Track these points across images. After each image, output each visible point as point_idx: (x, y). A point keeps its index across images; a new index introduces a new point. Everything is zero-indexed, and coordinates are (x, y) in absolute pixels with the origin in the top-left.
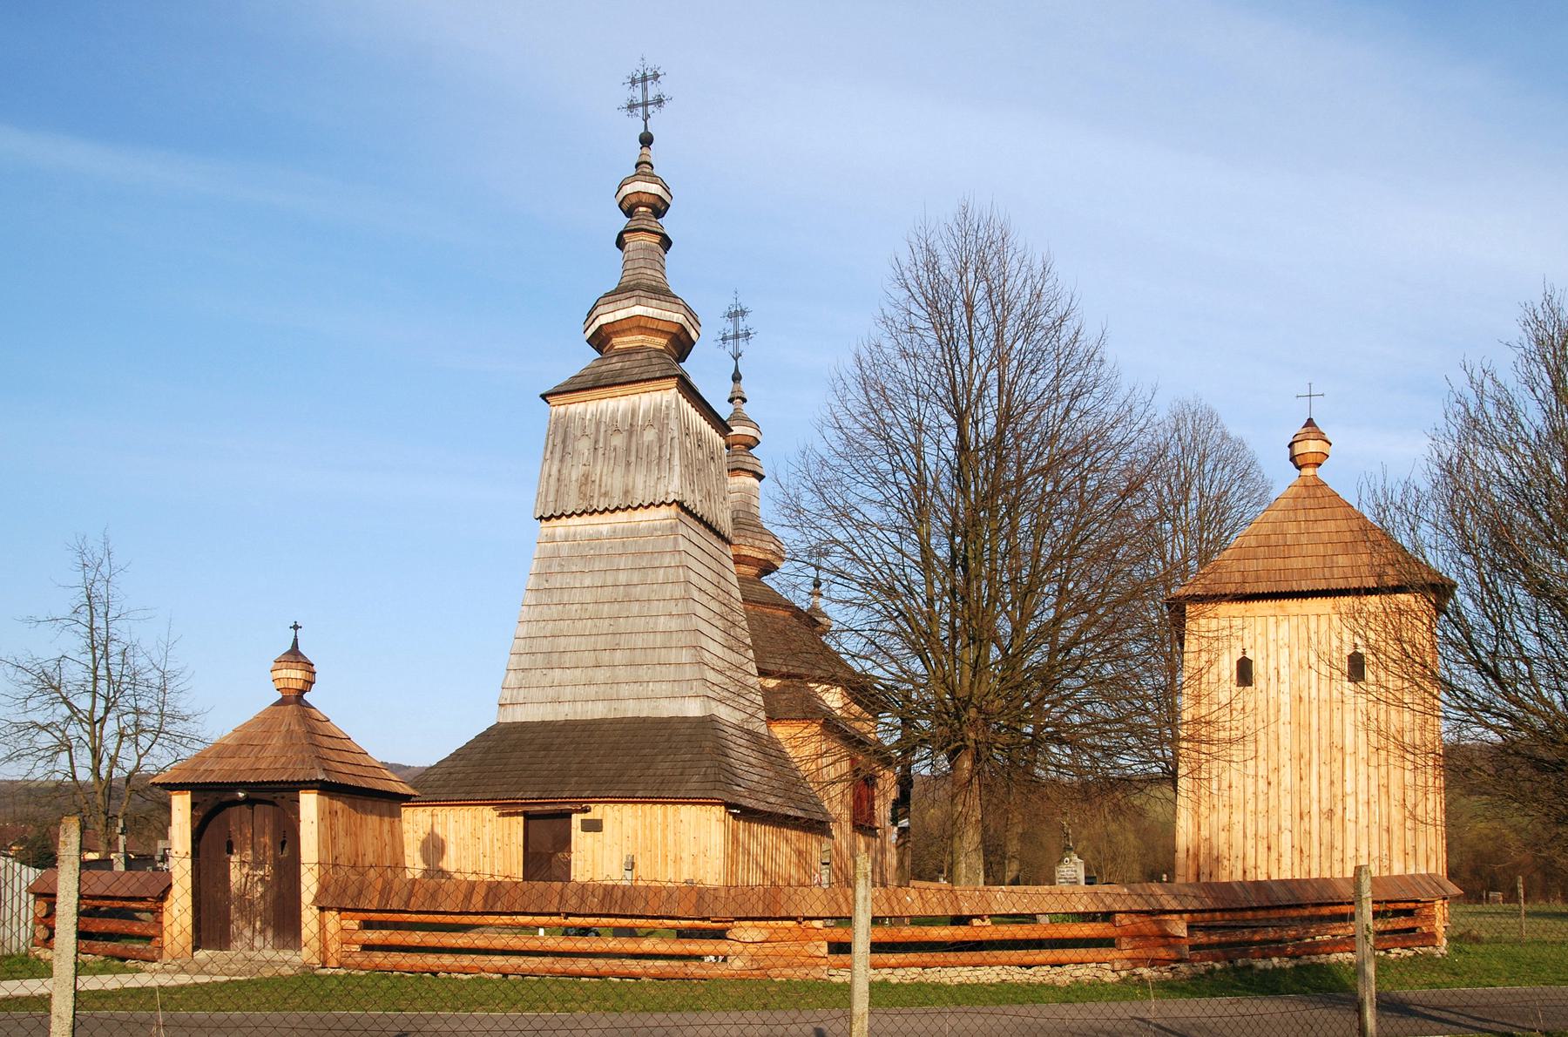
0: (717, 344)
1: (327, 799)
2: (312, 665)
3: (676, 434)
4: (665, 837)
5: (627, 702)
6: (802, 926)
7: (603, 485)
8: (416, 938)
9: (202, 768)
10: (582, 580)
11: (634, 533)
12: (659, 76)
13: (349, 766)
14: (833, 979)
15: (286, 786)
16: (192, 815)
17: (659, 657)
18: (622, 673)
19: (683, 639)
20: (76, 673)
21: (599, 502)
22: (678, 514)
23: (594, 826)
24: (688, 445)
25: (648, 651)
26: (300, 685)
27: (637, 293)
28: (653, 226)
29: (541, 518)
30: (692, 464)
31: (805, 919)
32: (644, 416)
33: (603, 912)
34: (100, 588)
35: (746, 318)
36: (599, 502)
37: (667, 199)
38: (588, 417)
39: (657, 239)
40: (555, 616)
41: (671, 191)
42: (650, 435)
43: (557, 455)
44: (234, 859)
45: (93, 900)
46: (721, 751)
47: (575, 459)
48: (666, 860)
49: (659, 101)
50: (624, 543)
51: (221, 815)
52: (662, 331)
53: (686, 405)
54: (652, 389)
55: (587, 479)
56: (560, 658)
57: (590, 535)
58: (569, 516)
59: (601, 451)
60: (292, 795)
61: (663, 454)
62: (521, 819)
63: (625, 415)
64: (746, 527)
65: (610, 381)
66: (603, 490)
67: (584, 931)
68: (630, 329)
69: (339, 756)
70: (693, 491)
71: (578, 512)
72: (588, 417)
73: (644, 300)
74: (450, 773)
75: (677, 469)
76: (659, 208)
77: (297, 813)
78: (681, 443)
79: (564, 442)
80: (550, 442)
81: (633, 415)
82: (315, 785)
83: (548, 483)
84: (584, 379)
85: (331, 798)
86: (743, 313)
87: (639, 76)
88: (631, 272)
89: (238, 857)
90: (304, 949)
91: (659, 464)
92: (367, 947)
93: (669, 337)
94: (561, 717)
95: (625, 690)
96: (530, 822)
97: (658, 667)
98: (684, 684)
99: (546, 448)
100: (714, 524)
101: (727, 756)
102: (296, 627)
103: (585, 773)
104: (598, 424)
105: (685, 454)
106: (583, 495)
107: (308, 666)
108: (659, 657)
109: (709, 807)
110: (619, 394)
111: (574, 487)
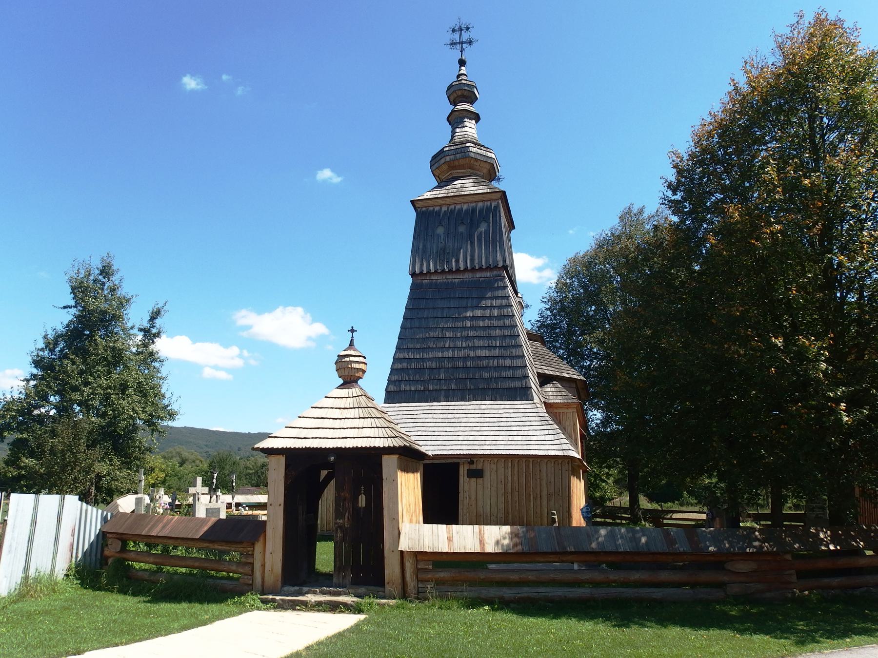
45: (152, 525)
49: (470, 42)
55: (444, 252)
87: (457, 28)
102: (352, 331)
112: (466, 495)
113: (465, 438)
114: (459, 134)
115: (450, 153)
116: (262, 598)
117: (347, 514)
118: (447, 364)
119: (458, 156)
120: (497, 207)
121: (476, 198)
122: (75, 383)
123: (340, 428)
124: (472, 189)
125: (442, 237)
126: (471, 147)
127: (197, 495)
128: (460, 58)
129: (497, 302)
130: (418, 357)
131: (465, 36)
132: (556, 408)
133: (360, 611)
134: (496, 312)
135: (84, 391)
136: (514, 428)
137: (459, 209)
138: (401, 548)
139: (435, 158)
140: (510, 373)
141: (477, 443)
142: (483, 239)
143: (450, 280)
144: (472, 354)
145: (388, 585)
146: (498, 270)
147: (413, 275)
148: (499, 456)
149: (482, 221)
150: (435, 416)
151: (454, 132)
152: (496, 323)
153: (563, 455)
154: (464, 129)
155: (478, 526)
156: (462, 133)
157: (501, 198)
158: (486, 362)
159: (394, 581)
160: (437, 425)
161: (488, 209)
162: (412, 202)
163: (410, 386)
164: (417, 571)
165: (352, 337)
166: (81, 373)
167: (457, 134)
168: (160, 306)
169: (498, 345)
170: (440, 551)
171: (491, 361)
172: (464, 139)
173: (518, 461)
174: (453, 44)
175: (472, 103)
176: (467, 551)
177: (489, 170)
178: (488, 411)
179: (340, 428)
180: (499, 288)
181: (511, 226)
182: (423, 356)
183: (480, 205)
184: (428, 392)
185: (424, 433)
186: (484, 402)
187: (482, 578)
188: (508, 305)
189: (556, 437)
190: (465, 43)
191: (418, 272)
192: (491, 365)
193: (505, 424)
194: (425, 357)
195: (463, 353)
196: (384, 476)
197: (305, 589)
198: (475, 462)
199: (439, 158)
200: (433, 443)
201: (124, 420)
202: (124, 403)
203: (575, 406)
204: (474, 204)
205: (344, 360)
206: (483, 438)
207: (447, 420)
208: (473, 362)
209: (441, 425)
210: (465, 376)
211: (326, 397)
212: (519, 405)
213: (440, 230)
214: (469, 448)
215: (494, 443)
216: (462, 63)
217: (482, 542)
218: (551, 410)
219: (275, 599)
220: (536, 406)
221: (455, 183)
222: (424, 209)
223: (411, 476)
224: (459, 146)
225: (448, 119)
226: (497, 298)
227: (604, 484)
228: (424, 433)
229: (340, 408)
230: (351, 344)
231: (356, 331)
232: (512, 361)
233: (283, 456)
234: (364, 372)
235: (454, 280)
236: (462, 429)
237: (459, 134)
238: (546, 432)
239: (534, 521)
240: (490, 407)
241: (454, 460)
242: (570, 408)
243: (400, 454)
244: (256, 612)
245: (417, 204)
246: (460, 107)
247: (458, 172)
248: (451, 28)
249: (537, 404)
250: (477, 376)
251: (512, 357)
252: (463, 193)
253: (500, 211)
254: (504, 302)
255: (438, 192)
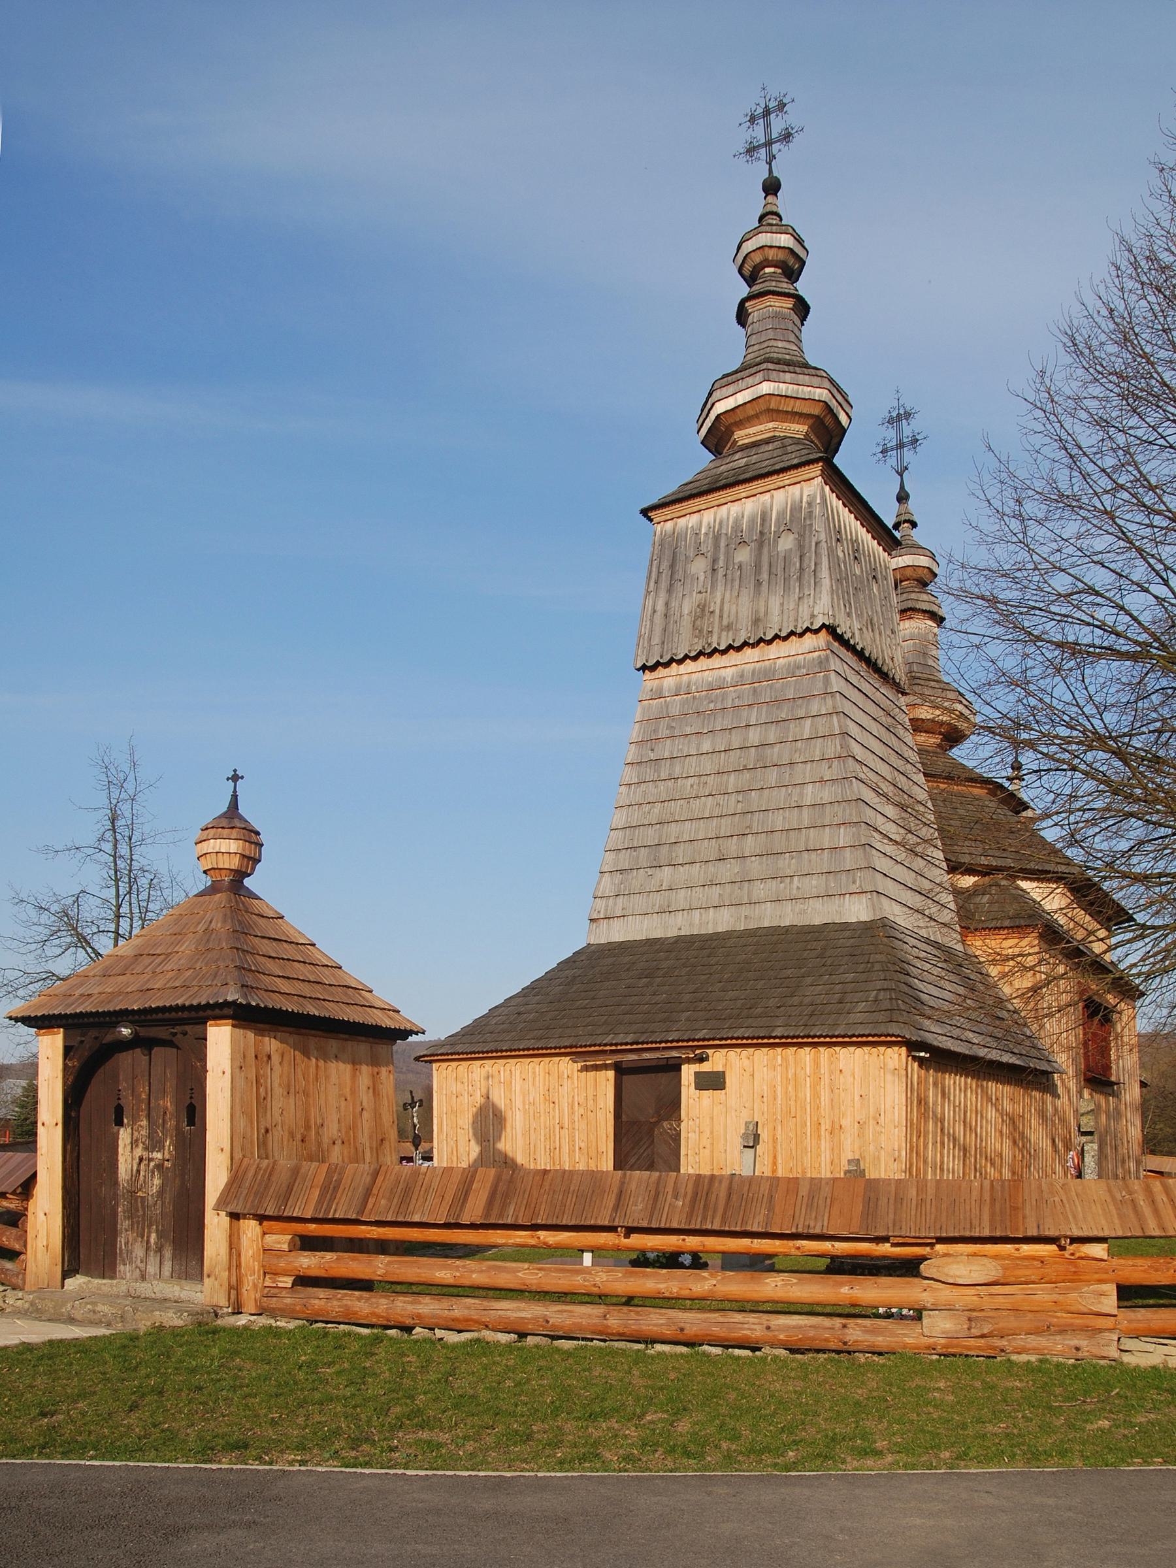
0: (876, 458)
1: (251, 1035)
2: (258, 833)
3: (823, 537)
4: (816, 1095)
5: (763, 906)
6: (1067, 1254)
7: (725, 616)
8: (379, 1266)
9: (78, 993)
10: (698, 745)
11: (768, 675)
12: (785, 105)
13: (297, 984)
14: (1126, 1358)
15: (186, 1015)
16: (65, 1066)
17: (807, 840)
18: (755, 867)
19: (840, 814)
20: (93, 911)
21: (719, 638)
22: (828, 644)
23: (713, 1082)
24: (841, 555)
25: (791, 833)
26: (234, 863)
27: (764, 366)
28: (785, 286)
29: (644, 668)
30: (847, 579)
31: (1075, 1240)
32: (778, 519)
33: (692, 1226)
34: (125, 809)
35: (912, 421)
36: (719, 638)
37: (802, 254)
38: (703, 531)
39: (789, 303)
40: (664, 797)
41: (806, 244)
42: (787, 543)
43: (664, 585)
44: (124, 1135)
46: (900, 968)
47: (688, 586)
48: (819, 1130)
49: (787, 136)
50: (755, 690)
51: (109, 1065)
52: (801, 415)
53: (836, 503)
54: (788, 482)
55: (703, 610)
56: (670, 852)
57: (710, 684)
58: (680, 662)
59: (721, 572)
60: (198, 1028)
61: (805, 566)
62: (611, 1074)
63: (752, 521)
64: (922, 682)
65: (732, 480)
66: (725, 622)
67: (671, 1261)
68: (757, 416)
69: (282, 968)
70: (849, 615)
71: (693, 654)
72: (703, 531)
73: (774, 375)
74: (519, 1014)
75: (826, 583)
76: (792, 267)
77: (203, 1058)
78: (831, 552)
79: (672, 566)
80: (654, 569)
81: (763, 520)
82: (227, 1011)
83: (652, 621)
84: (698, 484)
85: (260, 1032)
86: (908, 415)
87: (760, 110)
88: (756, 348)
89: (129, 1130)
90: (206, 1280)
91: (800, 579)
92: (304, 1281)
93: (810, 421)
94: (672, 933)
95: (760, 890)
96: (625, 1077)
97: (805, 855)
98: (844, 876)
99: (649, 578)
100: (880, 662)
101: (908, 974)
102: (235, 778)
103: (703, 1005)
104: (717, 538)
105: (834, 564)
106: (697, 631)
107: (251, 836)
108: (807, 840)
109: (882, 1049)
110: (744, 495)
111: (686, 622)
125: (702, 578)
131: (778, 125)
190: (776, 142)
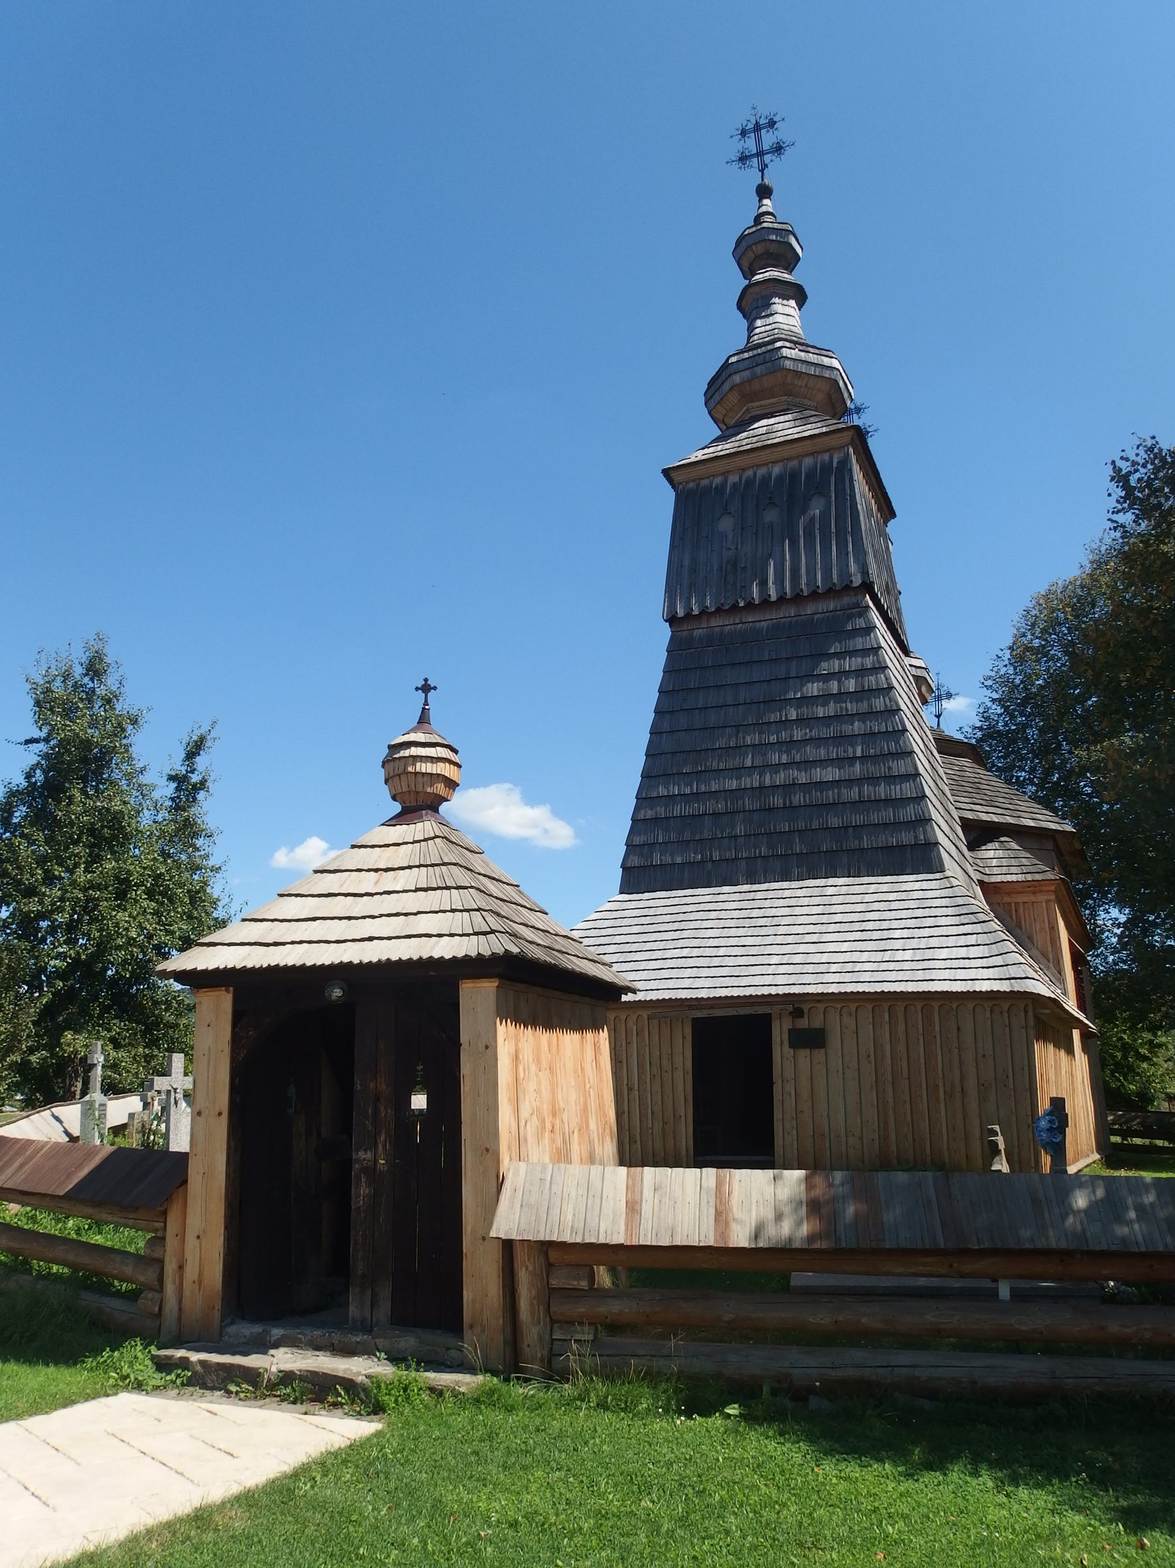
35: (863, 416)
49: (778, 149)
87: (750, 126)
102: (426, 688)
112: (790, 1088)
113: (785, 959)
114: (763, 329)
115: (742, 366)
116: (158, 1356)
117: (383, 1137)
118: (748, 804)
119: (758, 370)
120: (845, 463)
121: (799, 448)
122: (27, 879)
123: (364, 917)
124: (790, 431)
125: (730, 537)
126: (784, 349)
127: (172, 1093)
128: (760, 182)
129: (849, 664)
130: (688, 791)
131: (768, 139)
132: (1009, 894)
133: (376, 1409)
134: (851, 685)
135: (44, 894)
136: (897, 934)
137: (763, 476)
138: (498, 1230)
139: (714, 383)
140: (888, 815)
141: (810, 968)
142: (817, 532)
143: (751, 624)
144: (803, 778)
145: (470, 1332)
146: (852, 593)
147: (672, 620)
148: (857, 997)
149: (813, 495)
150: (723, 915)
151: (751, 328)
152: (851, 707)
153: (1011, 991)
154: (771, 320)
155: (714, 1170)
156: (768, 328)
157: (852, 443)
158: (833, 793)
159: (485, 1322)
160: (726, 932)
161: (826, 468)
162: (666, 473)
163: (672, 855)
164: (549, 1295)
165: (426, 703)
166: (42, 861)
167: (757, 331)
168: (203, 731)
169: (859, 754)
170: (602, 1240)
171: (844, 791)
172: (772, 337)
173: (905, 1007)
174: (743, 159)
175: (790, 269)
176: (678, 1242)
177: (830, 396)
178: (840, 899)
179: (364, 917)
180: (857, 632)
181: (887, 511)
182: (697, 790)
183: (808, 462)
184: (710, 865)
185: (696, 952)
186: (831, 881)
187: (726, 1319)
188: (877, 666)
189: (995, 949)
191: (680, 613)
192: (844, 798)
193: (877, 925)
194: (703, 790)
195: (782, 776)
196: (464, 1038)
197: (277, 1333)
198: (806, 1011)
199: (720, 381)
200: (713, 972)
201: (119, 948)
202: (122, 916)
203: (1053, 888)
204: (795, 463)
205: (397, 756)
206: (825, 958)
207: (747, 923)
208: (804, 796)
209: (733, 932)
210: (789, 826)
211: (353, 847)
212: (910, 882)
213: (726, 524)
214: (792, 979)
215: (849, 967)
216: (764, 192)
217: (722, 1217)
218: (997, 898)
219: (187, 1359)
220: (950, 882)
221: (756, 426)
222: (691, 485)
223: (569, 1041)
224: (759, 351)
225: (740, 306)
226: (853, 653)
227: (1145, 1065)
228: (696, 952)
229: (376, 870)
230: (424, 719)
231: (435, 688)
232: (893, 787)
233: (227, 991)
234: (452, 784)
235: (758, 624)
236: (779, 939)
237: (763, 329)
238: (972, 940)
239: (949, 1149)
240: (844, 890)
241: (756, 1008)
242: (1041, 891)
243: (500, 976)
244: (127, 1399)
245: (673, 475)
246: (761, 276)
247: (761, 406)
248: (738, 130)
249: (951, 879)
250: (815, 825)
251: (891, 779)
252: (769, 442)
253: (851, 470)
254: (869, 662)
255: (719, 448)
